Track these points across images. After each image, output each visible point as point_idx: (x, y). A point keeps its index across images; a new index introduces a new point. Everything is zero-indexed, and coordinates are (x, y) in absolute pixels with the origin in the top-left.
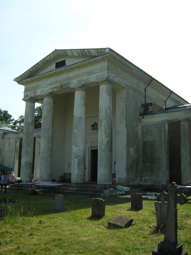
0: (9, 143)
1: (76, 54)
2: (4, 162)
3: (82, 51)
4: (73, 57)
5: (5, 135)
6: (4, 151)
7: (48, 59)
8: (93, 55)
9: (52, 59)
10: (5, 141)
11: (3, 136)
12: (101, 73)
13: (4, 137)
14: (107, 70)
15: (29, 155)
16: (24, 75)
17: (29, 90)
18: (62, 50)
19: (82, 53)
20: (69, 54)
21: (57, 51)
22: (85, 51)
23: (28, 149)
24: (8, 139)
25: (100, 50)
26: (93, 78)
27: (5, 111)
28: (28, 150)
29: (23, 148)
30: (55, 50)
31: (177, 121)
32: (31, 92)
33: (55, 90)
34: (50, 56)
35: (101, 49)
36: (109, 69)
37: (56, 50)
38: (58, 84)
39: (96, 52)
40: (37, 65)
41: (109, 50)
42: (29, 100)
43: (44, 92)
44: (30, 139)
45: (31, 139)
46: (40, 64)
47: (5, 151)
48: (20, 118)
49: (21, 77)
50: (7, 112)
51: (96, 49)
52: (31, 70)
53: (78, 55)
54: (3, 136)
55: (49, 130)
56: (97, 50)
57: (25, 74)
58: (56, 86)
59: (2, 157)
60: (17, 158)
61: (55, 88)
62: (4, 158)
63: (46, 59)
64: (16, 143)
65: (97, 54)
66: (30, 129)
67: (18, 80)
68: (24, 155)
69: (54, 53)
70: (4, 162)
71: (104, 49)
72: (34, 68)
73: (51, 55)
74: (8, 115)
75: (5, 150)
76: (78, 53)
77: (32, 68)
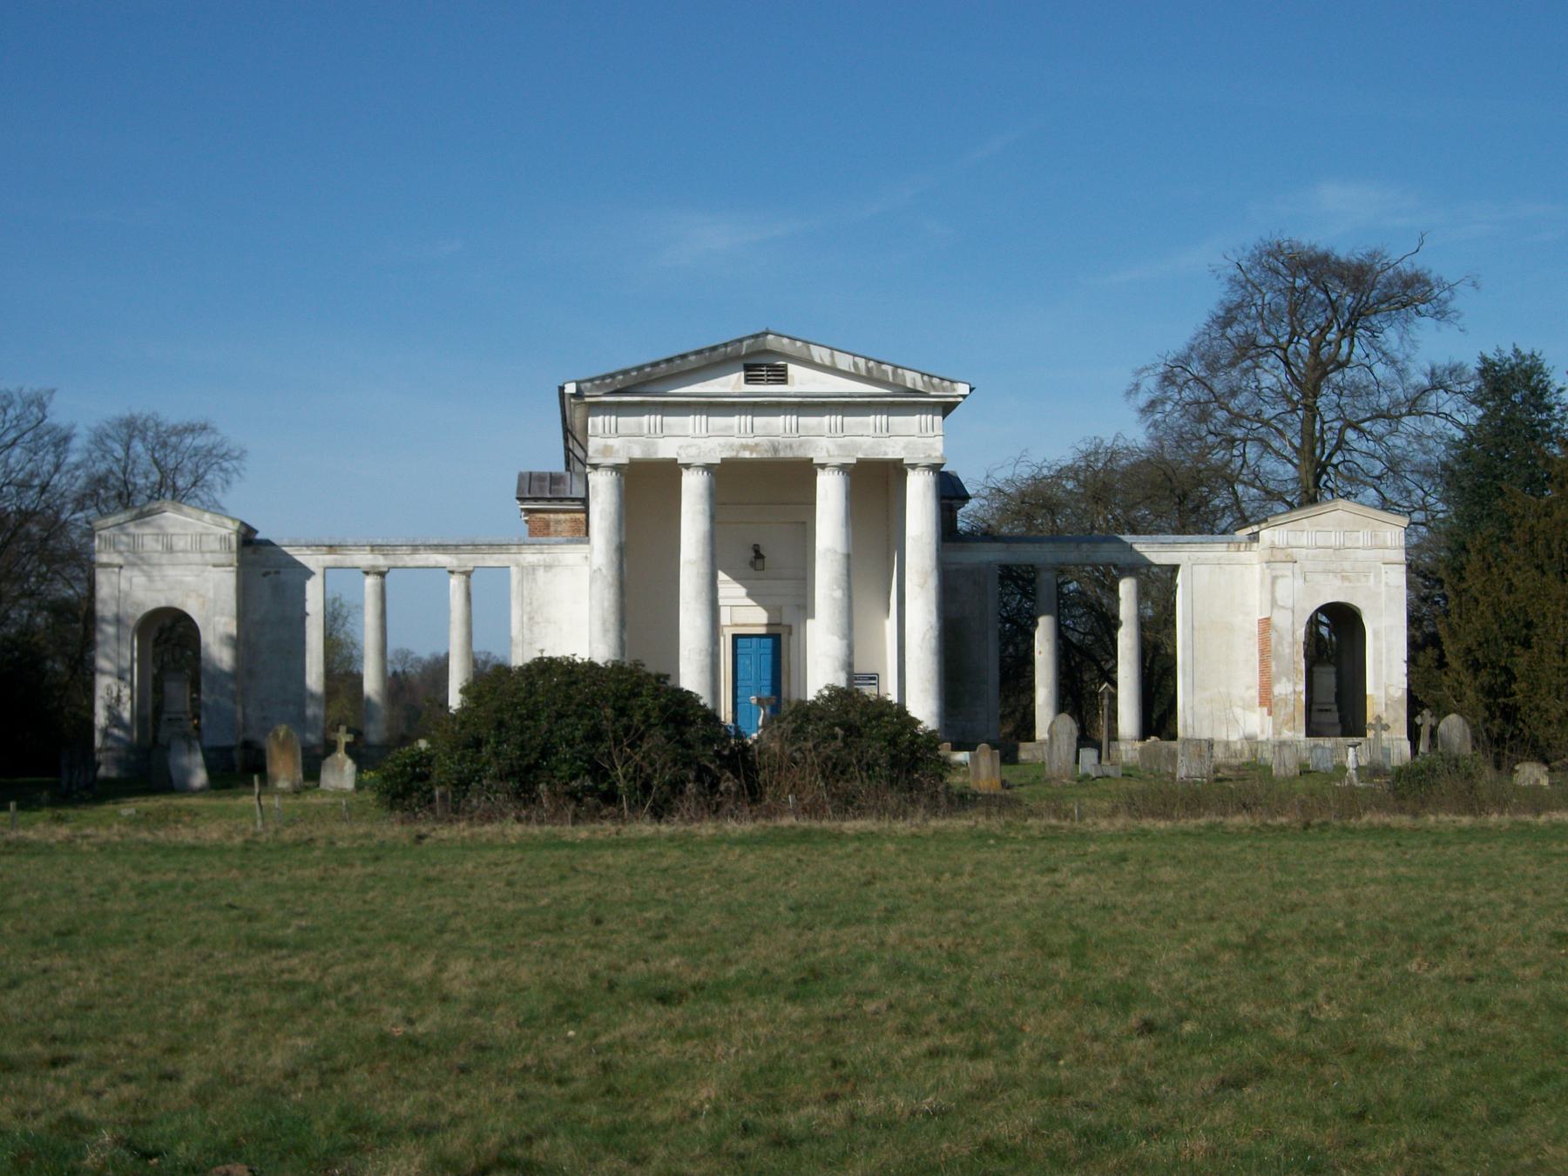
8: (909, 385)
19: (869, 370)
24: (266, 570)
26: (666, 449)
33: (747, 455)
38: (757, 440)
43: (693, 451)
58: (751, 441)
61: (745, 447)
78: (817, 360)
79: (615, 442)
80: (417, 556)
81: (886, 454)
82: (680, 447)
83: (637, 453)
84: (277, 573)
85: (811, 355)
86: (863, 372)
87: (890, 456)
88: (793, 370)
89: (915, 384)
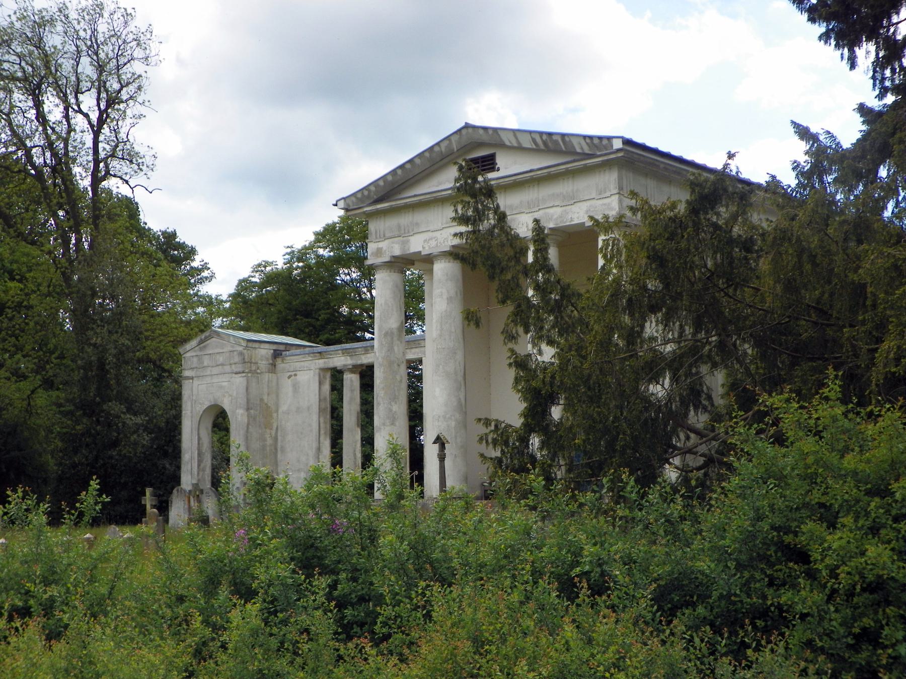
0: (296, 387)
1: (527, 143)
2: (282, 447)
3: (544, 137)
4: (520, 149)
5: (279, 361)
6: (277, 411)
7: (443, 149)
9: (455, 150)
10: (278, 379)
11: (271, 362)
12: (600, 202)
13: (274, 365)
14: (619, 193)
15: (397, 424)
16: (369, 191)
17: (384, 236)
18: (485, 129)
19: (545, 143)
20: (507, 139)
21: (470, 130)
22: (554, 138)
23: (395, 408)
24: (290, 374)
25: (596, 141)
27: (164, 233)
28: (394, 410)
29: (379, 404)
30: (463, 124)
31: (253, 601)
32: (393, 243)
34: (450, 140)
35: (600, 138)
36: (622, 189)
37: (467, 126)
39: (587, 143)
40: (408, 166)
41: (623, 143)
42: (388, 264)
43: (433, 243)
44: (398, 378)
45: (401, 377)
46: (418, 161)
47: (280, 411)
48: (257, 272)
49: (359, 195)
50: (174, 235)
51: (585, 137)
52: (390, 178)
53: (534, 147)
54: (271, 362)
55: (455, 353)
56: (588, 140)
57: (373, 188)
59: (273, 432)
60: (325, 433)
62: (279, 434)
63: (437, 149)
64: (320, 383)
65: (590, 150)
66: (396, 348)
67: (349, 205)
68: (384, 424)
69: (461, 134)
70: (282, 447)
71: (609, 138)
72: (399, 172)
73: (453, 139)
74: (182, 246)
75: (283, 408)
76: (534, 141)
77: (393, 172)
78: (508, 143)
79: (384, 245)
80: (368, 355)
81: (572, 220)
82: (425, 241)
83: (397, 252)
84: (295, 375)
85: (501, 139)
86: (542, 146)
87: (576, 222)
88: (500, 161)
89: (582, 148)
